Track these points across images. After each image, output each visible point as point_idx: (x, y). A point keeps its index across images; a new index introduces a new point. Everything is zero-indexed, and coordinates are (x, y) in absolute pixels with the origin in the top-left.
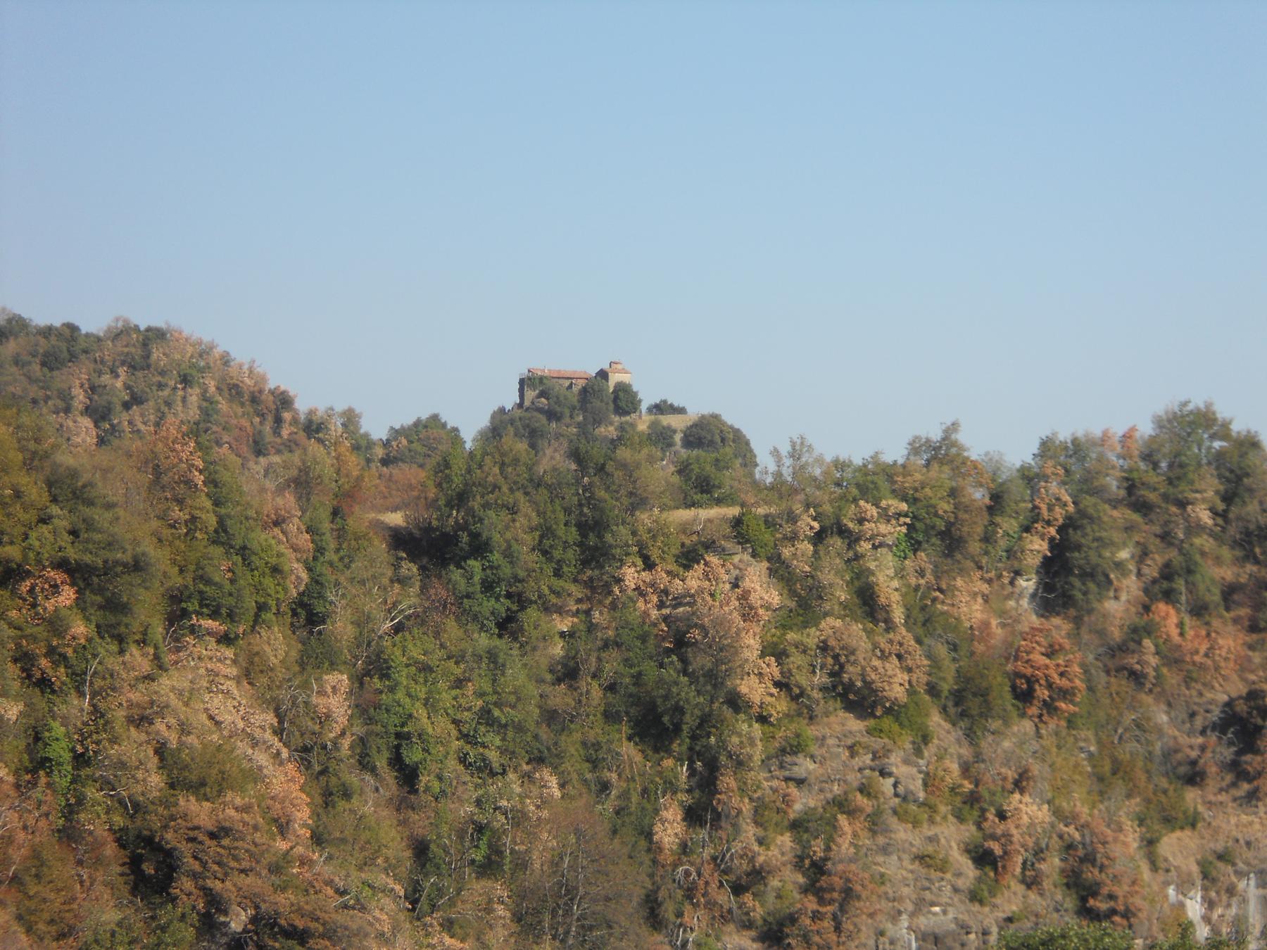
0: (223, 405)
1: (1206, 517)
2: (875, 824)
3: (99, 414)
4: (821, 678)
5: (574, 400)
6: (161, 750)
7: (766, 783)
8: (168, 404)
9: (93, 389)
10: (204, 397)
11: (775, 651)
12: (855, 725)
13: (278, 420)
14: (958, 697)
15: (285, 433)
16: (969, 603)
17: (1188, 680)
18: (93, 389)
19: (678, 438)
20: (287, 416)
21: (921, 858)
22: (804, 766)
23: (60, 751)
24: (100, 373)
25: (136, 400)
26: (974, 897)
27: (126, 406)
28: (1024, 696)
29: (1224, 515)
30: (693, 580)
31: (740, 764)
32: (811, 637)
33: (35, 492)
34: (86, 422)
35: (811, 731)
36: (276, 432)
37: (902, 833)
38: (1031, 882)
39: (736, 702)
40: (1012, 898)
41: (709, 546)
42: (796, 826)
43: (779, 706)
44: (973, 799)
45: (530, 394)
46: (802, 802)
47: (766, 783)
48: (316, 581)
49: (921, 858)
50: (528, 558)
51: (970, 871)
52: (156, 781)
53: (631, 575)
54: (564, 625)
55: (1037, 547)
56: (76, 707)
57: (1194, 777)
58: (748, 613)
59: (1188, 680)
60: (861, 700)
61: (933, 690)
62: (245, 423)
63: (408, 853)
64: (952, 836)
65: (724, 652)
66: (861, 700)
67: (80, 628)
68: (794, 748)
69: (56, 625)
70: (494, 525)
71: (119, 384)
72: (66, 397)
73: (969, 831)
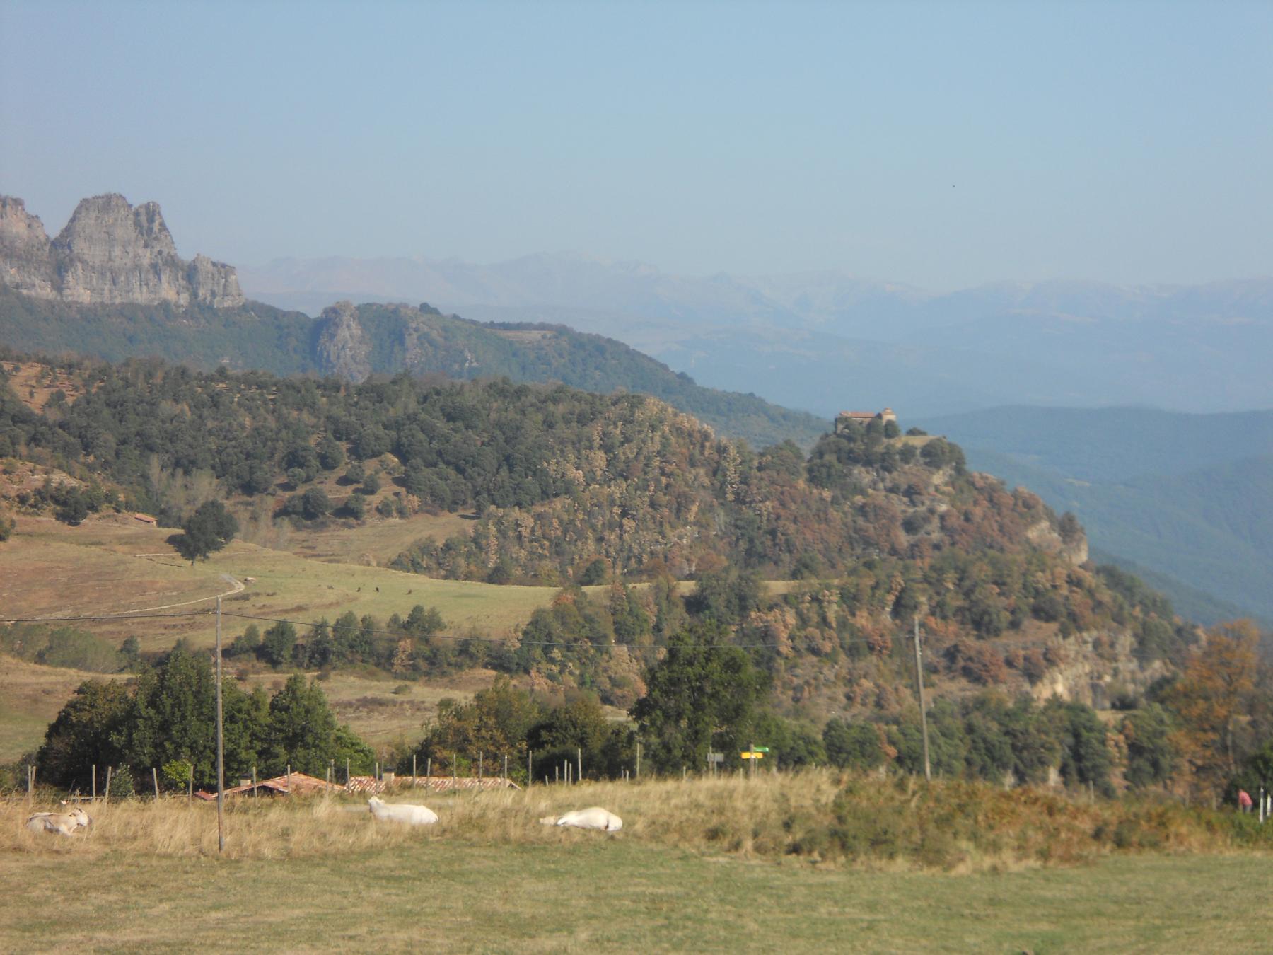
0: (673, 440)
1: (951, 586)
2: (817, 688)
3: (607, 448)
4: (804, 646)
5: (862, 430)
6: (610, 678)
7: (787, 676)
8: (644, 442)
9: (604, 434)
10: (663, 436)
11: (792, 638)
12: (814, 659)
13: (703, 446)
14: (850, 650)
15: (706, 453)
16: (862, 620)
17: (938, 640)
18: (604, 434)
19: (918, 452)
20: (707, 444)
21: (830, 698)
22: (799, 671)
23: (588, 679)
24: (608, 425)
25: (627, 440)
26: (845, 709)
27: (622, 444)
28: (871, 648)
29: (959, 586)
30: (770, 617)
31: (778, 671)
32: (803, 633)
33: (581, 621)
34: (601, 454)
35: (800, 661)
36: (702, 454)
37: (825, 691)
38: (864, 704)
39: (779, 653)
40: (857, 708)
41: (777, 605)
42: (794, 689)
43: (791, 654)
44: (850, 681)
45: (840, 427)
46: (796, 681)
47: (787, 676)
48: (659, 619)
49: (830, 698)
50: (723, 609)
51: (844, 701)
52: (609, 686)
53: (753, 614)
54: (734, 628)
55: (891, 598)
56: (591, 670)
57: (935, 671)
58: (786, 626)
59: (938, 640)
60: (815, 651)
61: (842, 647)
62: (684, 450)
63: (123, 805)
64: (840, 692)
65: (775, 638)
66: (815, 651)
67: (592, 651)
68: (795, 666)
69: (586, 651)
70: (712, 600)
71: (618, 432)
72: (590, 441)
73: (847, 690)
